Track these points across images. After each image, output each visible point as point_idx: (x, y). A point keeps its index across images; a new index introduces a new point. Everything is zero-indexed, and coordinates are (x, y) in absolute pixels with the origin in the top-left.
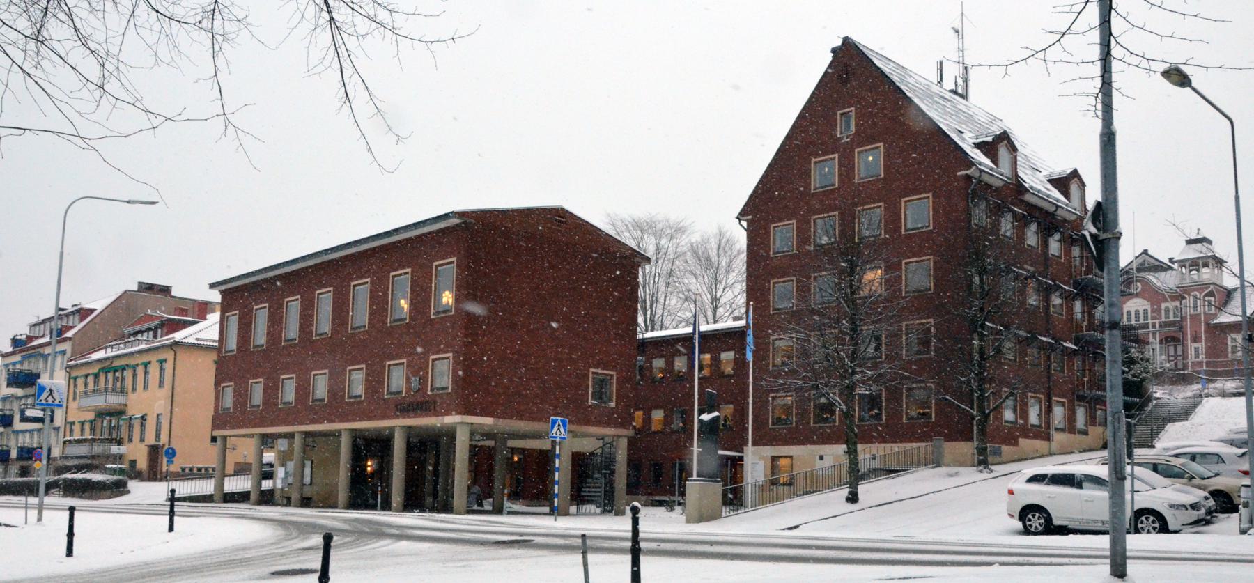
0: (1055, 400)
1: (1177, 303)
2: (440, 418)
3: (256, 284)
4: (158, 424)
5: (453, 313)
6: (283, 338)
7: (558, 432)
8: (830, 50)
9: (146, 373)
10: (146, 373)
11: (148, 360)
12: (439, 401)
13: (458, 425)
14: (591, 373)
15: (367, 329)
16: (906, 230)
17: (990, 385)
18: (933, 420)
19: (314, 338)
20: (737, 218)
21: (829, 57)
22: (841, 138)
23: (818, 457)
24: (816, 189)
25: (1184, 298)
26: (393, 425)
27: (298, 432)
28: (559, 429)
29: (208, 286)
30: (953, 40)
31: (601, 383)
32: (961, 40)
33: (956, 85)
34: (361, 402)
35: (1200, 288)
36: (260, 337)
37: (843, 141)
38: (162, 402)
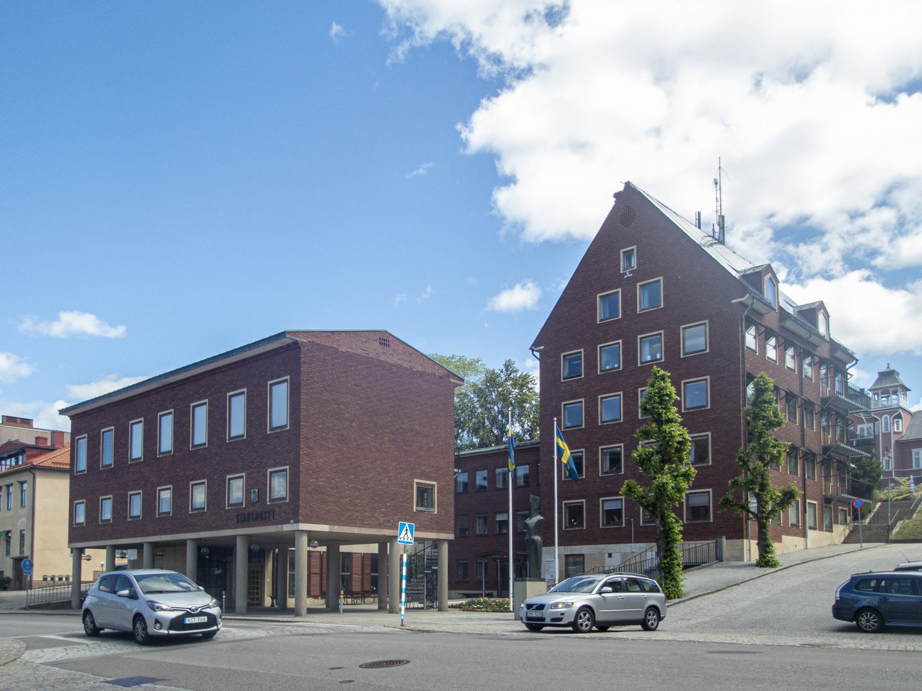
0: (809, 503)
1: (871, 425)
2: (280, 526)
3: (100, 409)
4: (22, 536)
5: (288, 428)
6: (129, 458)
7: (406, 537)
8: (613, 195)
9: (9, 494)
10: (9, 494)
11: (11, 483)
12: (277, 510)
13: (296, 532)
14: (415, 483)
15: (207, 446)
16: (684, 354)
17: (665, 501)
18: (711, 521)
19: (158, 456)
20: (531, 349)
21: (612, 202)
22: (625, 274)
23: (607, 555)
24: (601, 320)
25: (877, 420)
26: (235, 534)
27: (146, 542)
28: (406, 533)
29: (58, 412)
30: (712, 193)
31: (423, 492)
32: (718, 192)
33: (714, 232)
34: (203, 514)
35: (890, 412)
36: (108, 458)
37: (625, 277)
38: (24, 519)
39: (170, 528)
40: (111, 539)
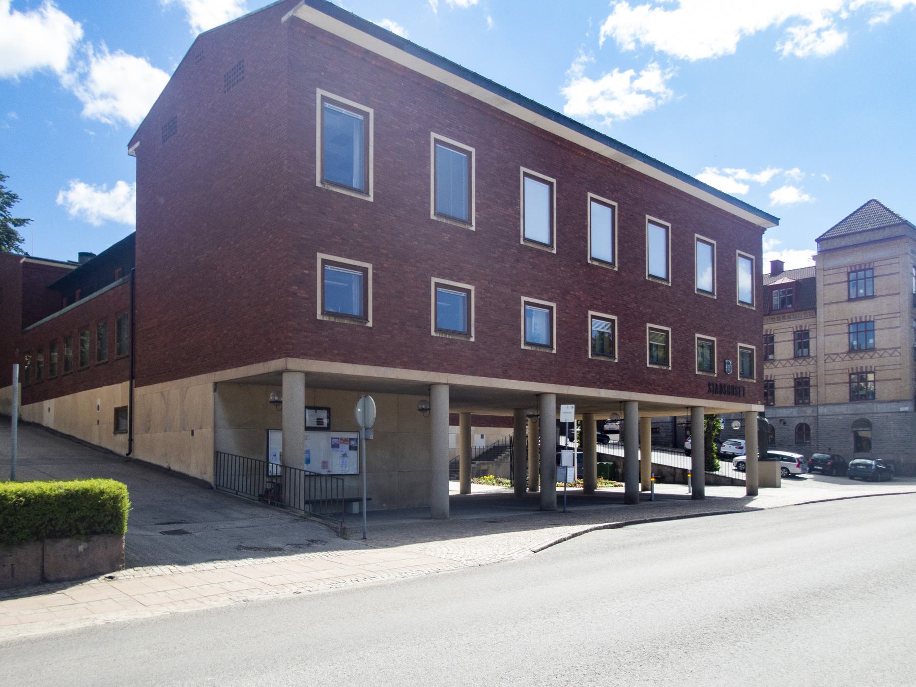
39: (616, 381)
40: (473, 374)
